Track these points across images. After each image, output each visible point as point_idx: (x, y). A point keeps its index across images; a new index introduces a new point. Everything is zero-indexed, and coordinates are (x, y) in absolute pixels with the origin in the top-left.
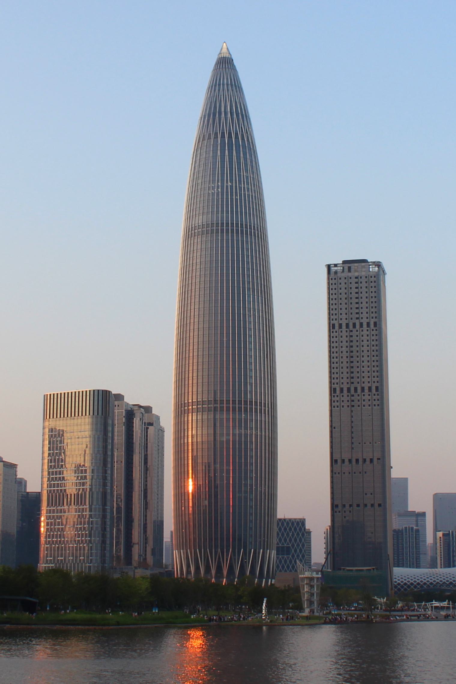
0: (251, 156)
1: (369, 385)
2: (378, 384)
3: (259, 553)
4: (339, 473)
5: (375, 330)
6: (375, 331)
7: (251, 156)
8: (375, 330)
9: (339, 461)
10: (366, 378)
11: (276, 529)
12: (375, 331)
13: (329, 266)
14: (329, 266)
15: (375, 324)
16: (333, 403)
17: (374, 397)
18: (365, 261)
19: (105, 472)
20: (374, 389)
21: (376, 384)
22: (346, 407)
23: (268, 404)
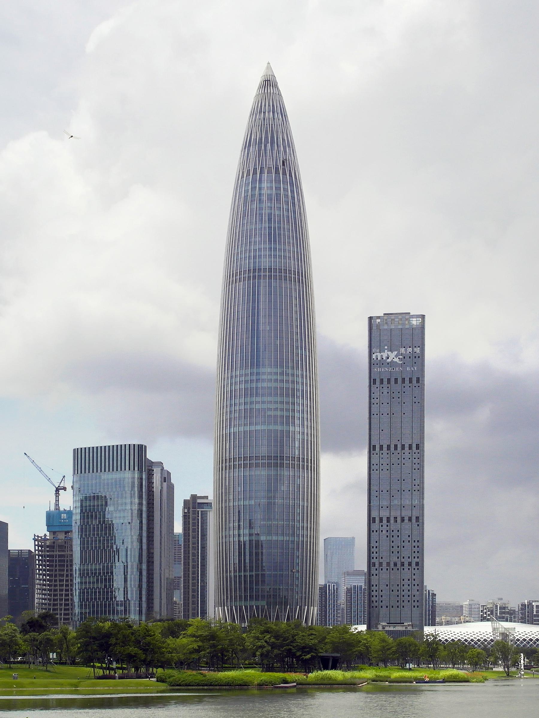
0: (298, 195)
1: (410, 560)
2: (418, 560)
3: (304, 609)
4: (377, 531)
5: (416, 569)
6: (417, 459)
7: (298, 195)
8: (416, 569)
9: (377, 520)
10: (406, 586)
11: (317, 591)
12: (417, 459)
13: (370, 318)
14: (370, 318)
15: (417, 564)
16: (372, 394)
17: (414, 456)
18: (409, 313)
19: (198, 685)
20: (414, 565)
21: (416, 560)
22: (385, 470)
23: (314, 461)
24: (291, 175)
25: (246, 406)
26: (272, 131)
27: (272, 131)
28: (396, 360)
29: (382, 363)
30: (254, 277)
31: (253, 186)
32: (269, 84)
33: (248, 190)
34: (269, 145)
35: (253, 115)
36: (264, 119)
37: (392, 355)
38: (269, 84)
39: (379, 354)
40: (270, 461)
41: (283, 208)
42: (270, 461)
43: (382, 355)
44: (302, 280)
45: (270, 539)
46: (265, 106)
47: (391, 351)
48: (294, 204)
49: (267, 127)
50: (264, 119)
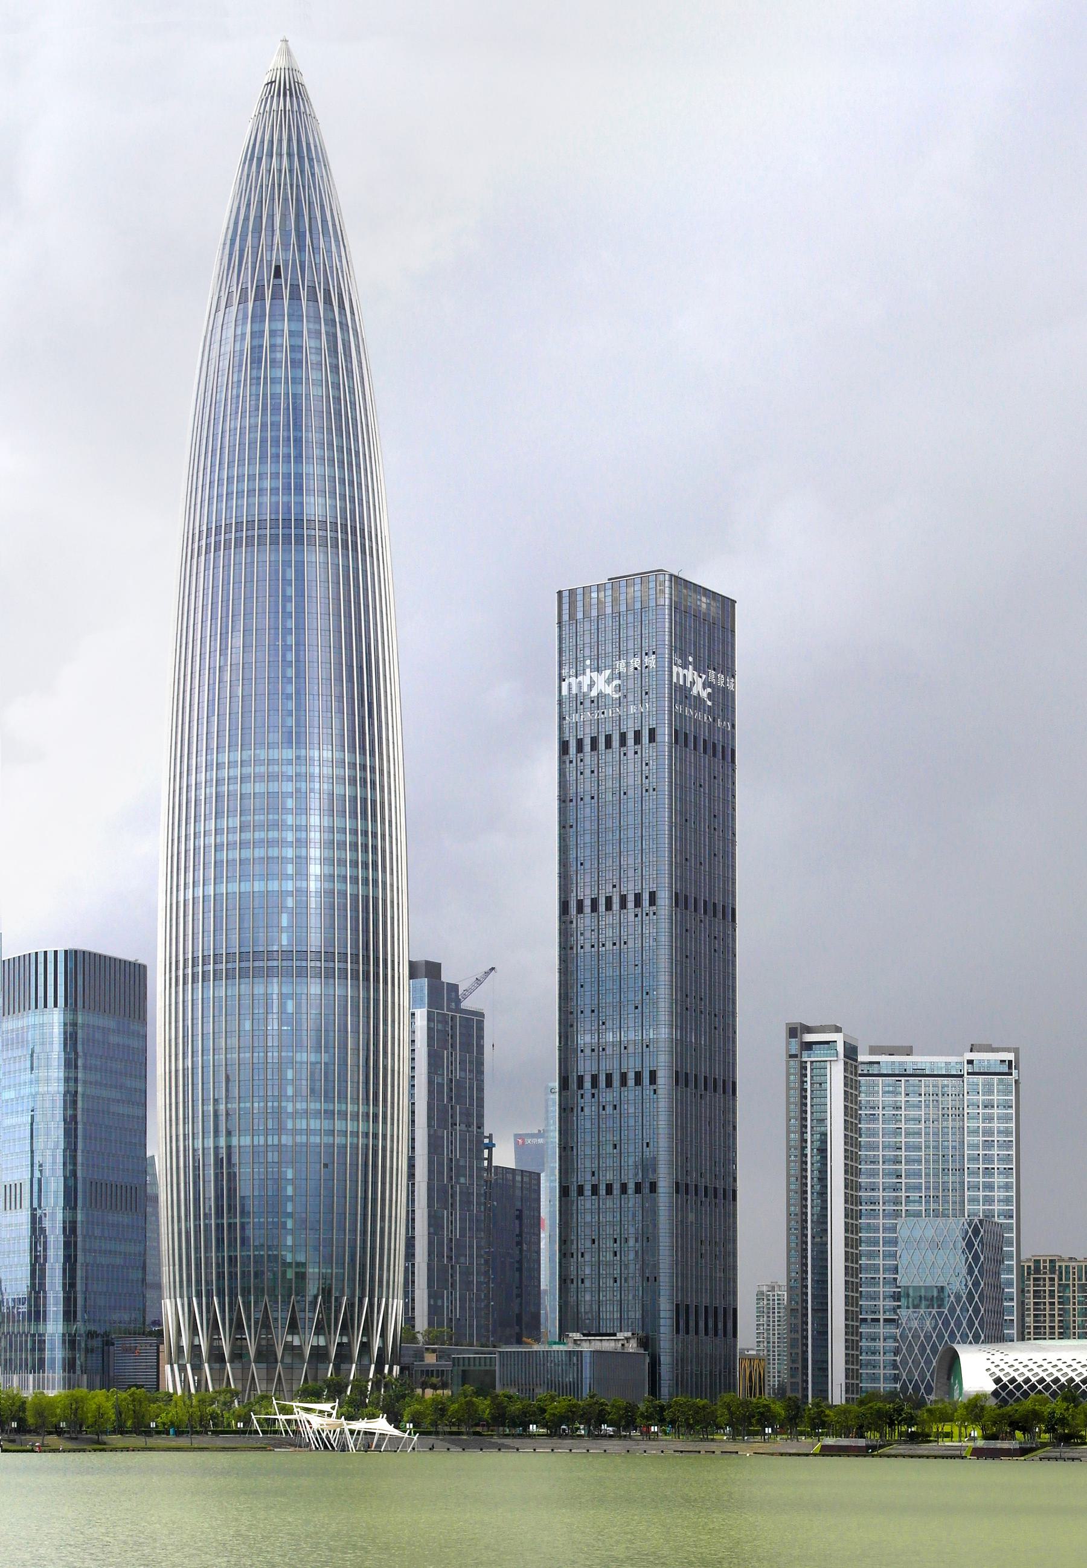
24: (342, 306)
25: (230, 836)
26: (298, 200)
27: (298, 200)
28: (609, 690)
29: (580, 701)
30: (240, 494)
31: (257, 328)
32: (288, 92)
33: (243, 335)
34: (288, 98)
35: (251, 160)
36: (280, 171)
37: (601, 679)
38: (288, 92)
39: (573, 680)
40: (299, 963)
41: (327, 381)
42: (299, 963)
43: (580, 683)
44: (354, 543)
45: (299, 882)
46: (280, 140)
47: (598, 670)
48: (350, 372)
49: (285, 193)
50: (280, 171)
